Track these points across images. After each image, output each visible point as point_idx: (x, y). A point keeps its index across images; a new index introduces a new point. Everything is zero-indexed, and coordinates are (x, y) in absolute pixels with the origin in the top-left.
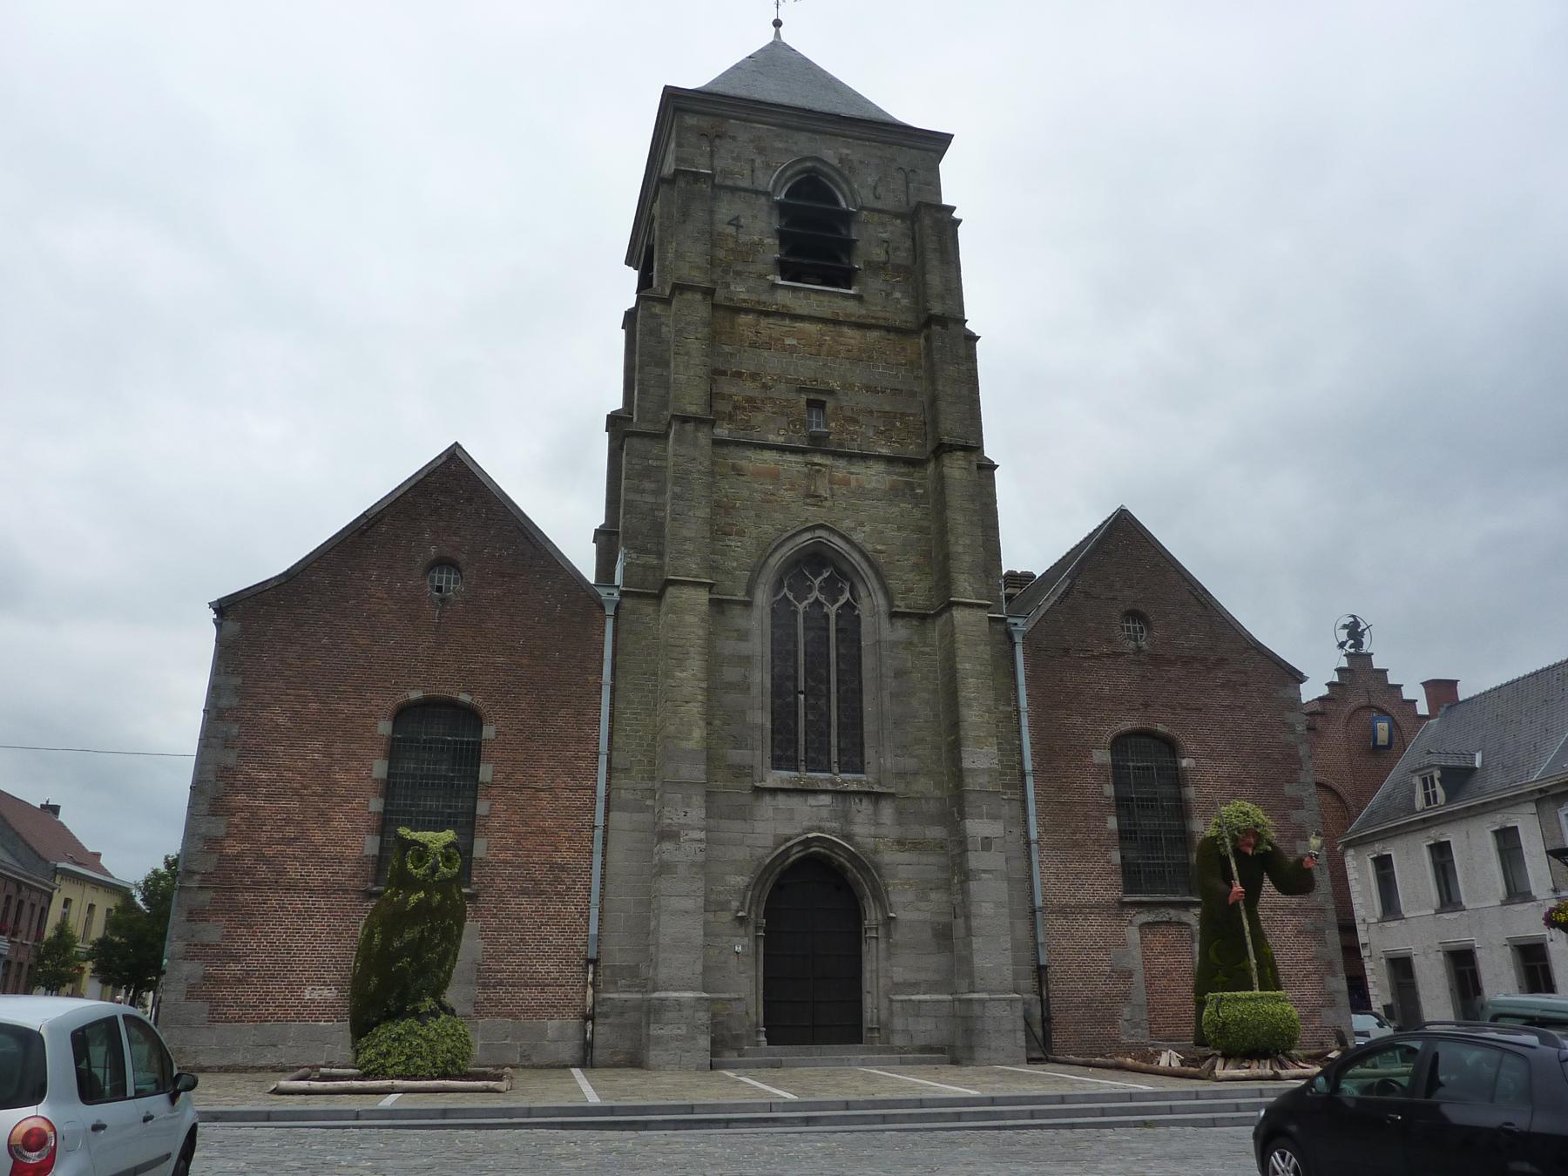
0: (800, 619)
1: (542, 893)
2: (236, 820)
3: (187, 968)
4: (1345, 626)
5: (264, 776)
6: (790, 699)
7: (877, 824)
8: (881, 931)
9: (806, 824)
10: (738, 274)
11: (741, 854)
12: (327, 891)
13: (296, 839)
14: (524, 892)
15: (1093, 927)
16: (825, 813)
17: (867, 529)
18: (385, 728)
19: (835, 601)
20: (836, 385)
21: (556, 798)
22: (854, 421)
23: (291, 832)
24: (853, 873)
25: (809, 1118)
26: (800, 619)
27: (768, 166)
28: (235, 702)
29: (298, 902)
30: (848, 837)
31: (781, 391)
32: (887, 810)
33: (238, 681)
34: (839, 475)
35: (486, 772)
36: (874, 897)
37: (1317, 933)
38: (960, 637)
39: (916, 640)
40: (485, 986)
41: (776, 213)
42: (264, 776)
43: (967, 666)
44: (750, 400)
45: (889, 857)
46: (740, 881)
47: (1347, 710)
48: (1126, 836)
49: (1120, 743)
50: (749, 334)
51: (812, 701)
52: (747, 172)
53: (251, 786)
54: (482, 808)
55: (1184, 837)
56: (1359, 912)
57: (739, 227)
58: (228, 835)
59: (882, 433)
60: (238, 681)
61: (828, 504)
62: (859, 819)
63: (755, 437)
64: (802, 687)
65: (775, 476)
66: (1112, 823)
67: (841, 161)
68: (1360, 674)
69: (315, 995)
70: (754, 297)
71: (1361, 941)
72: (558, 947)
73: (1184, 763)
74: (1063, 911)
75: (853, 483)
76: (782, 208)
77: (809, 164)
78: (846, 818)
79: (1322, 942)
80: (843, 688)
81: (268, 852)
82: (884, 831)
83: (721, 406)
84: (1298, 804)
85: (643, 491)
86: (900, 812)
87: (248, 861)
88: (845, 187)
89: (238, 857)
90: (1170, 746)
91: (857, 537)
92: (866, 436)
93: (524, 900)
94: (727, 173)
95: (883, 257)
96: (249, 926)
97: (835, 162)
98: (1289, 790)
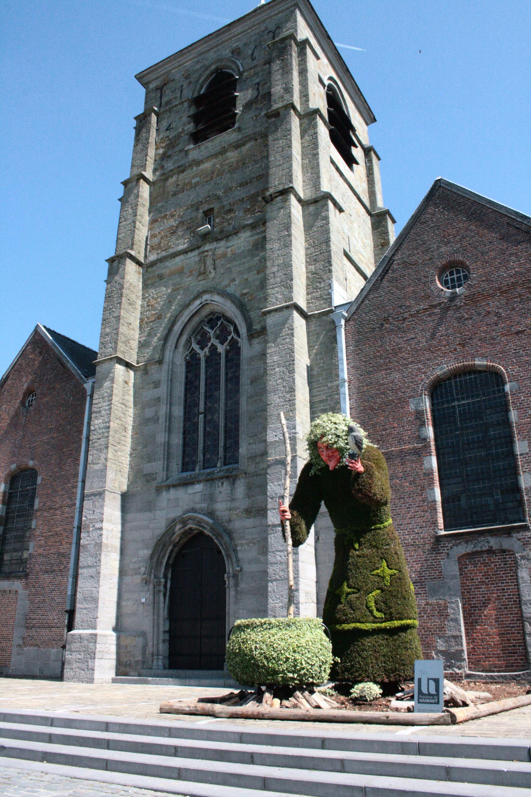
1: (54, 571)
7: (233, 500)
9: (185, 508)
14: (47, 572)
16: (198, 498)
17: (237, 282)
22: (230, 211)
30: (211, 514)
34: (219, 252)
35: (37, 504)
40: (27, 628)
49: (438, 389)
62: (220, 498)
68: (308, 449)
72: (58, 604)
77: (213, 67)
82: (237, 504)
93: (46, 576)
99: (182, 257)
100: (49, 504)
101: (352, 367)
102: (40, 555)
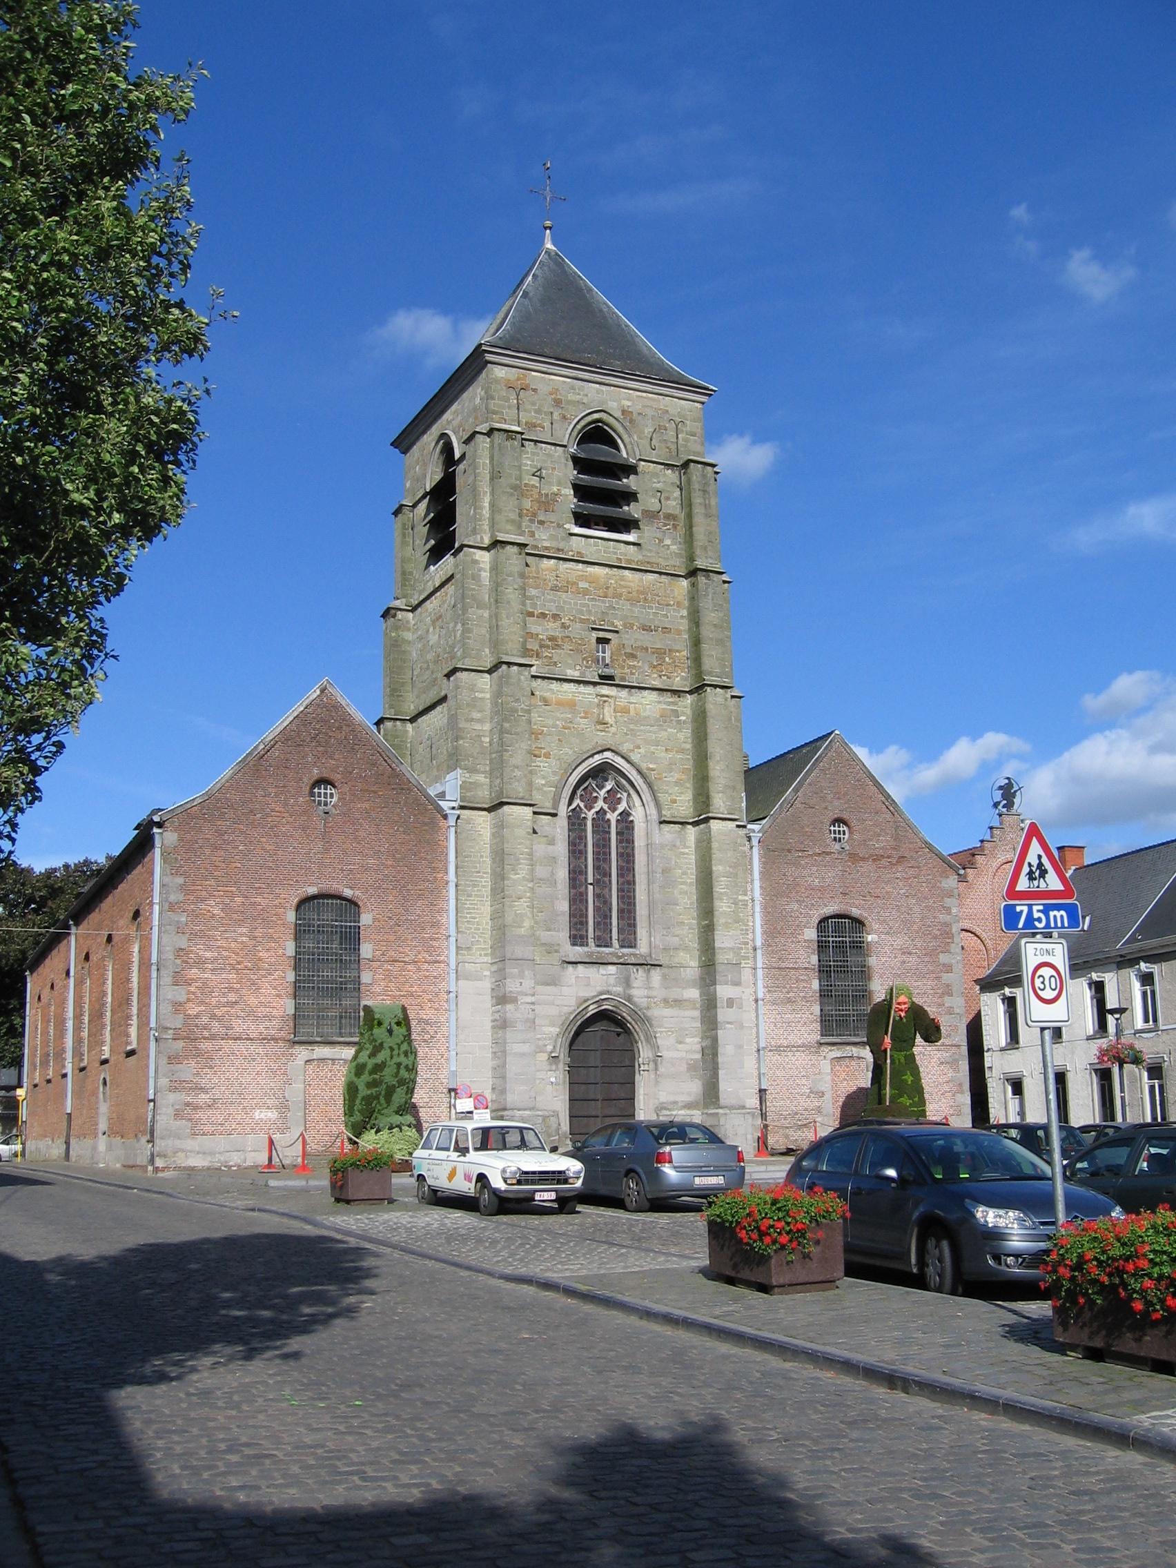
0: (589, 823)
2: (193, 989)
3: (172, 1097)
4: (1000, 788)
5: (208, 954)
6: (583, 889)
8: (652, 1066)
9: (599, 989)
10: (541, 523)
11: (553, 1011)
12: (265, 1039)
13: (236, 1003)
15: (801, 1059)
16: (612, 980)
18: (291, 916)
19: (614, 810)
20: (619, 624)
21: (419, 969)
22: (633, 656)
23: (232, 997)
24: (632, 1024)
25: (1048, 1101)
26: (589, 823)
27: (564, 417)
28: (181, 898)
29: (240, 1046)
31: (577, 630)
32: (656, 975)
33: (180, 880)
35: (366, 950)
36: (647, 1040)
37: (953, 1063)
38: (715, 845)
39: (678, 843)
41: (571, 464)
42: (208, 954)
43: (720, 868)
44: (552, 639)
45: (657, 1012)
46: (555, 1030)
47: (995, 865)
48: (824, 994)
50: (550, 577)
51: (598, 891)
52: (547, 424)
53: (200, 963)
54: (366, 977)
55: (865, 994)
56: (988, 1041)
57: (541, 477)
58: (189, 1000)
59: (655, 667)
60: (180, 880)
61: (613, 729)
63: (557, 672)
64: (590, 880)
65: (571, 705)
66: (816, 985)
67: (624, 412)
69: (262, 1116)
70: (554, 544)
71: (987, 1065)
73: (870, 938)
74: (778, 1049)
75: (632, 712)
76: (576, 461)
78: (627, 983)
79: (956, 1070)
80: (621, 880)
81: (218, 1013)
82: (654, 993)
83: (533, 645)
84: (948, 968)
85: (472, 720)
86: (664, 977)
87: (205, 1020)
88: (625, 437)
89: (197, 1016)
90: (858, 923)
91: (635, 757)
92: (641, 671)
94: (532, 426)
95: (657, 507)
96: (211, 1067)
97: (618, 414)
98: (943, 958)
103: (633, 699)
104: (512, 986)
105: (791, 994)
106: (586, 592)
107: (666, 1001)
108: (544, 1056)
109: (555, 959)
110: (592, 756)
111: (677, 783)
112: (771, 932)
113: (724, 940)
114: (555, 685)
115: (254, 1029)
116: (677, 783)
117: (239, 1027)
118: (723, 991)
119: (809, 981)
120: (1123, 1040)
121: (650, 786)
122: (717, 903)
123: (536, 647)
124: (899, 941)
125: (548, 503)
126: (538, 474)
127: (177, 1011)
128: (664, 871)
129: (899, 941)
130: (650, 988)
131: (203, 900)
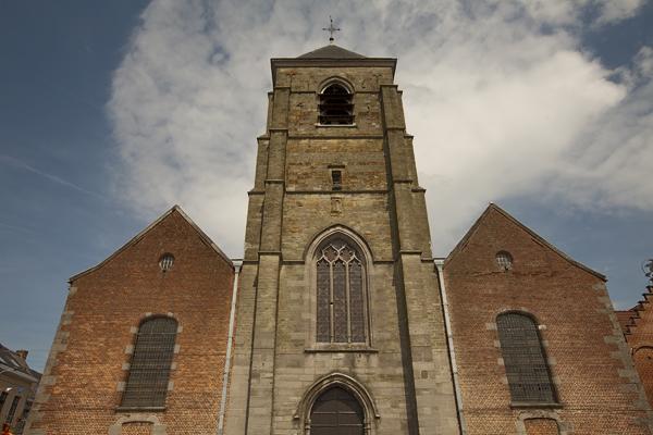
5: (77, 356)
9: (331, 368)
12: (98, 409)
16: (341, 363)
18: (134, 330)
20: (345, 163)
21: (208, 359)
22: (353, 177)
32: (374, 359)
33: (72, 313)
35: (177, 349)
38: (405, 269)
58: (57, 384)
60: (72, 313)
65: (317, 206)
74: (476, 412)
78: (353, 365)
86: (381, 360)
91: (357, 229)
99: (317, 196)
100: (191, 350)
101: (448, 297)
102: (181, 392)
103: (355, 198)
104: (257, 366)
105: (482, 370)
106: (325, 151)
107: (382, 376)
108: (290, 418)
109: (301, 349)
110: (328, 229)
111: (384, 240)
112: (460, 327)
113: (415, 330)
114: (306, 196)
115: (93, 403)
116: (384, 240)
117: (83, 401)
118: (418, 366)
119: (495, 359)
120: (396, 184)
121: (366, 243)
122: (409, 306)
123: (295, 178)
124: (565, 330)
125: (305, 116)
126: (300, 105)
127: (47, 392)
128: (378, 291)
129: (565, 330)
130: (368, 368)
131: (82, 323)
